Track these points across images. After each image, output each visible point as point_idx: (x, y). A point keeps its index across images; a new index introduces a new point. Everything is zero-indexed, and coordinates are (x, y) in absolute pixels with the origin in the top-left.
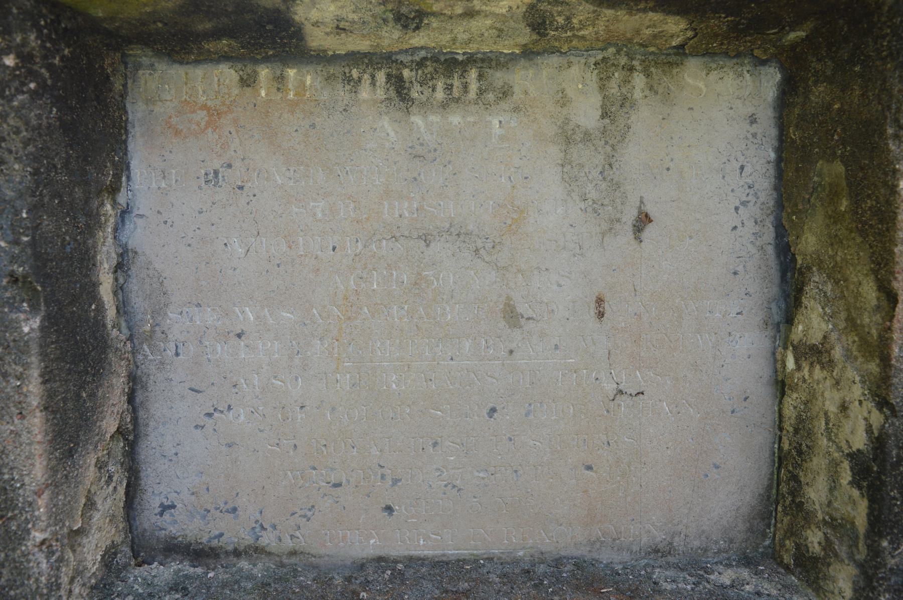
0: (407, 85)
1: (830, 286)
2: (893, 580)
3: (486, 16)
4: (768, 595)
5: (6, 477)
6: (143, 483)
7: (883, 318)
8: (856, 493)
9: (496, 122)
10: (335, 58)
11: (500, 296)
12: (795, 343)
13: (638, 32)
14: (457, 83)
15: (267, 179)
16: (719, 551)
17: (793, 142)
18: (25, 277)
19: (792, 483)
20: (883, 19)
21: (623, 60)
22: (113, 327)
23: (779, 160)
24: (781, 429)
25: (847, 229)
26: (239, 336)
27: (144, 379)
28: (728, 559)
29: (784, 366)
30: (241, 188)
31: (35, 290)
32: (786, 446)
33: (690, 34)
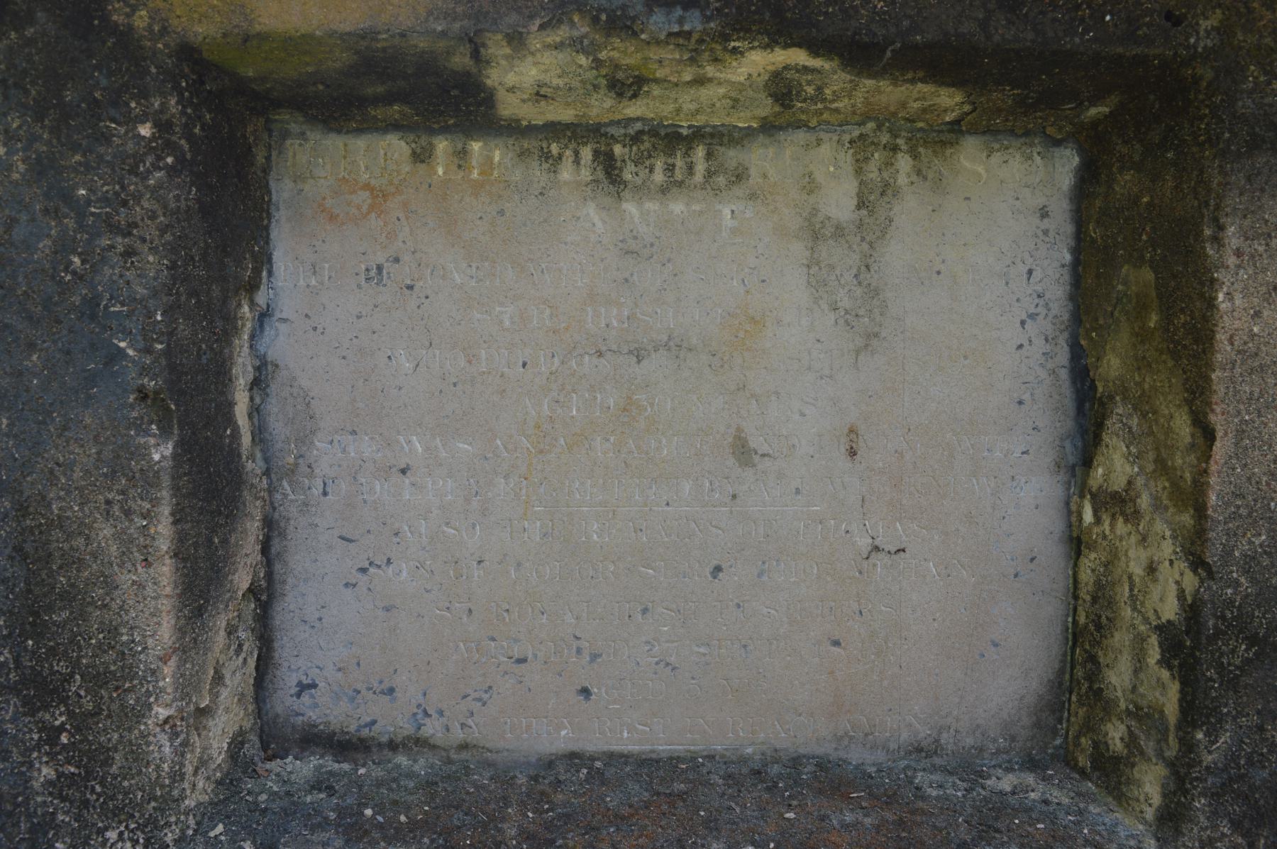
0: (618, 164)
1: (1136, 420)
2: (1210, 781)
3: (720, 84)
4: (1058, 804)
5: (125, 638)
6: (276, 655)
7: (1198, 459)
8: (1165, 674)
9: (727, 212)
10: (531, 130)
11: (729, 426)
12: (1094, 490)
13: (904, 105)
14: (679, 163)
15: (444, 277)
16: (998, 752)
17: (1093, 241)
18: (157, 393)
19: (1089, 666)
20: (1201, 97)
21: (885, 138)
22: (248, 458)
23: (1076, 263)
24: (1076, 597)
25: (1156, 350)
26: (403, 471)
27: (282, 524)
28: (1009, 761)
29: (1080, 519)
30: (410, 288)
31: (168, 409)
32: (1082, 620)
33: (967, 108)
